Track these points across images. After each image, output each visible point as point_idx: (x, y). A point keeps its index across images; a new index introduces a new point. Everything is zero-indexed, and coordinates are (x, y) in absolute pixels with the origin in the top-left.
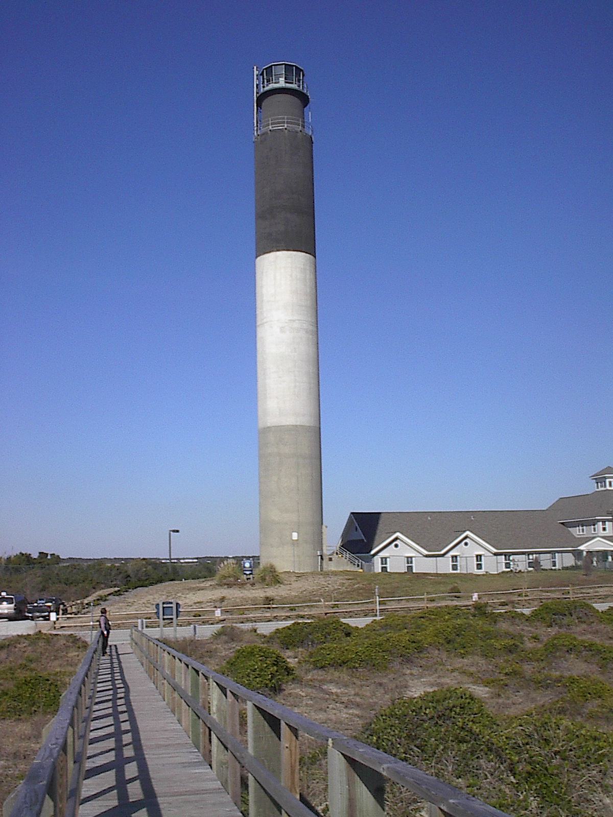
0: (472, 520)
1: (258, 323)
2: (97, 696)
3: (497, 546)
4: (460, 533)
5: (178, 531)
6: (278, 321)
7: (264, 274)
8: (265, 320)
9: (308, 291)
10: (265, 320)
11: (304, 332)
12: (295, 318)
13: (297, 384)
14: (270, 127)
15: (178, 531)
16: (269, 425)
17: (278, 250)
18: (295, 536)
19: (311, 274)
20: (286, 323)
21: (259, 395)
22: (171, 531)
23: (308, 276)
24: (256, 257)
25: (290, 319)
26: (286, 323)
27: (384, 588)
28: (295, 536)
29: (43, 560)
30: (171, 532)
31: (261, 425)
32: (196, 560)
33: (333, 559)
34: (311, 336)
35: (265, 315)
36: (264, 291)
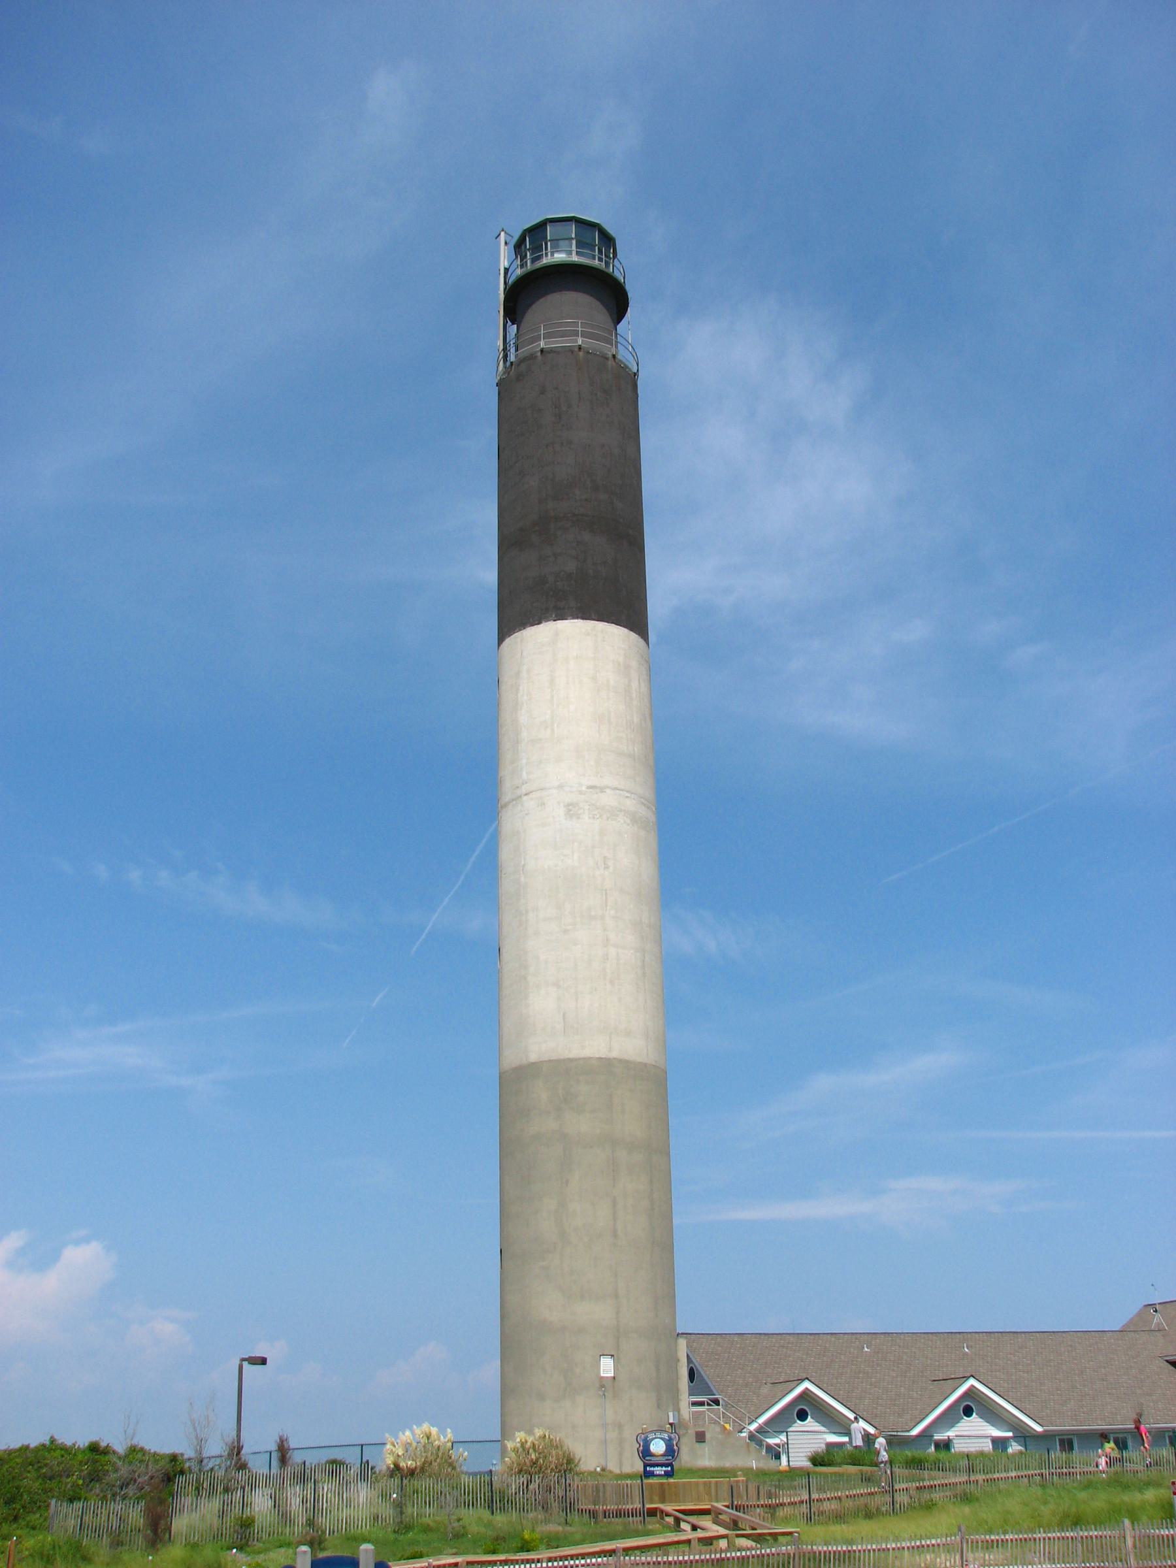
0: (967, 1354)
1: (506, 797)
2: (611, 270)
3: (1042, 1418)
4: (965, 1379)
5: (263, 1361)
6: (561, 787)
7: (524, 674)
8: (524, 789)
9: (636, 720)
10: (524, 789)
11: (628, 821)
12: (608, 781)
13: (612, 951)
14: (542, 344)
15: (263, 1361)
16: (533, 1057)
17: (562, 617)
18: (607, 1367)
19: (643, 685)
20: (581, 792)
21: (506, 983)
22: (243, 1360)
23: (635, 685)
24: (501, 640)
25: (590, 783)
26: (581, 792)
27: (818, 1515)
28: (607, 1367)
29: (90, 1486)
30: (245, 1364)
31: (511, 1058)
32: (202, 1482)
33: (708, 1436)
34: (643, 833)
35: (525, 775)
36: (523, 718)
